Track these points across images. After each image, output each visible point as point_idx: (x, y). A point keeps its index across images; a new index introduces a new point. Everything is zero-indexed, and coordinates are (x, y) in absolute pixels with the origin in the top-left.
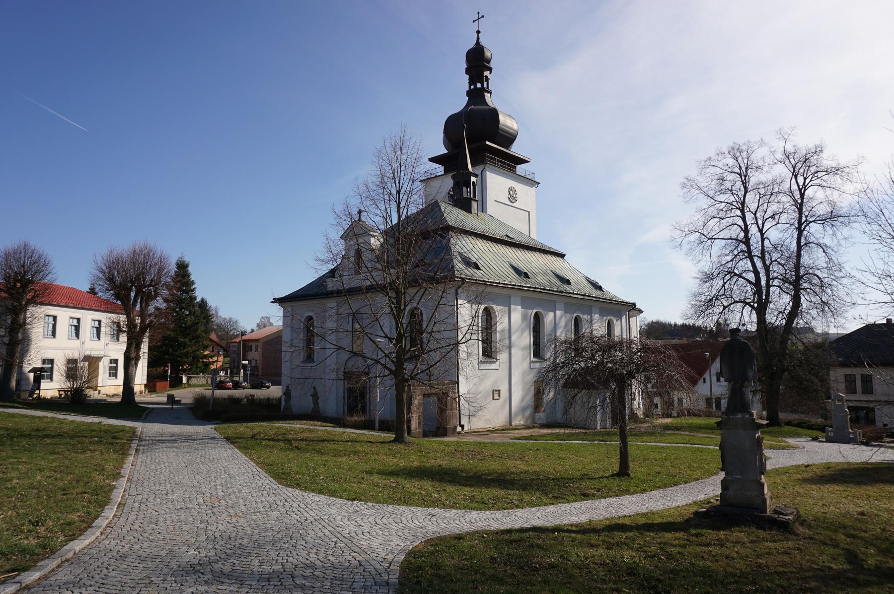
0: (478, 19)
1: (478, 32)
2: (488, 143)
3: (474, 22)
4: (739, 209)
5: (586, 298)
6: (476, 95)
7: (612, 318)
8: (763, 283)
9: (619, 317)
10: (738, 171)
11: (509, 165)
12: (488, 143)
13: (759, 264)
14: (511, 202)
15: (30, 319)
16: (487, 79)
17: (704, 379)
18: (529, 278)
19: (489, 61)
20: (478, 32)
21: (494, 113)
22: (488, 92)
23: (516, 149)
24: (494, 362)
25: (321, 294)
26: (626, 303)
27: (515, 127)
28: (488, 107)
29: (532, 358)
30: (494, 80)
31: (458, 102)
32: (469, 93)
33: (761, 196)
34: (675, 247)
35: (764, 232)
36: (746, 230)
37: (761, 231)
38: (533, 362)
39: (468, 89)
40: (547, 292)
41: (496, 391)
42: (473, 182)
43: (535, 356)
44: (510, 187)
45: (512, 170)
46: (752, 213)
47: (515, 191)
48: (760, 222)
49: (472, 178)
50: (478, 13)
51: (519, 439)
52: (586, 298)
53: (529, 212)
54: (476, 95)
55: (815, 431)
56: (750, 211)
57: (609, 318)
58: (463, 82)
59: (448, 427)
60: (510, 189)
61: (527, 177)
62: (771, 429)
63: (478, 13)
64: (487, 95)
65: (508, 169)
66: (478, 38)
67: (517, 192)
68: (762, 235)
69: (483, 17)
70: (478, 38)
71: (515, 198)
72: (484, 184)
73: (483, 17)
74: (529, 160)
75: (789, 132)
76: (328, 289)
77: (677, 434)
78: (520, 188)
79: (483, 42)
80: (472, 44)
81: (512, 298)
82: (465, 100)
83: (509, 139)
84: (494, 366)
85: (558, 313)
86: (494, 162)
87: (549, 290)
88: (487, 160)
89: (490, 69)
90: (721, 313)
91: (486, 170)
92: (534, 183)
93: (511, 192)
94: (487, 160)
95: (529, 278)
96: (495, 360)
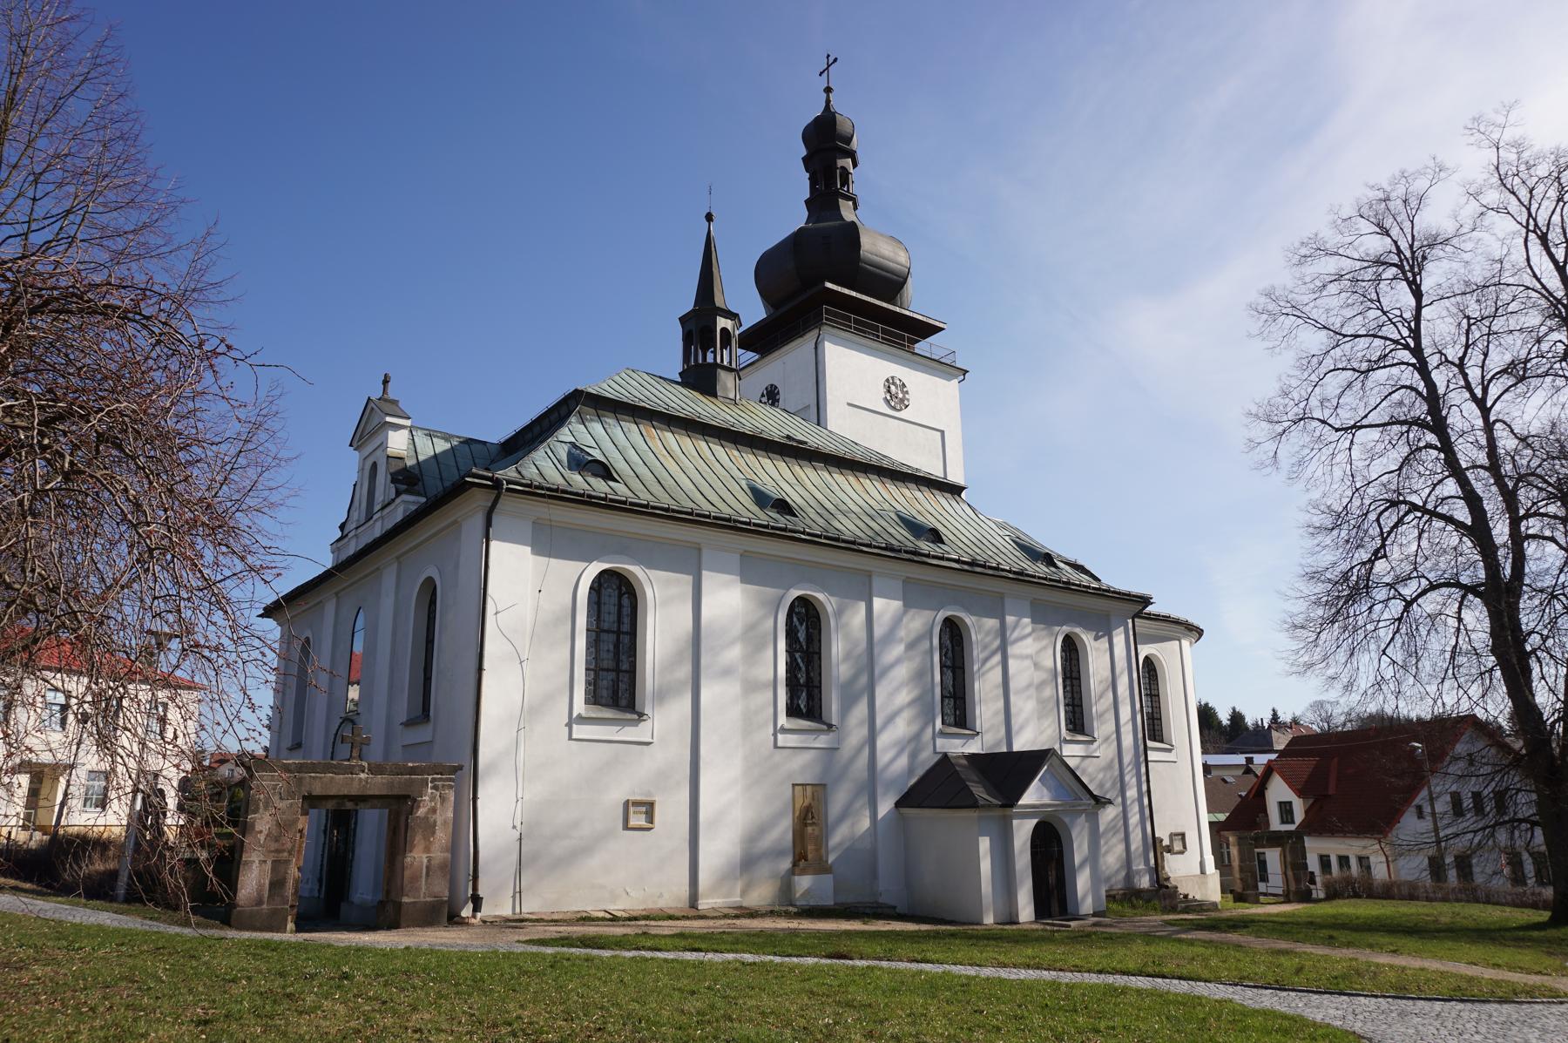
0: (827, 68)
1: (828, 90)
2: (829, 285)
4: (1406, 347)
5: (979, 569)
7: (1078, 630)
8: (1501, 531)
9: (1104, 629)
10: (1396, 260)
11: (856, 322)
12: (829, 285)
13: (1482, 483)
14: (894, 408)
17: (1419, 809)
18: (795, 516)
19: (849, 140)
20: (828, 90)
21: (852, 232)
22: (848, 198)
24: (635, 723)
26: (1119, 593)
27: (902, 258)
29: (783, 720)
30: (862, 179)
33: (1472, 321)
34: (1262, 465)
35: (1489, 404)
36: (1433, 398)
37: (1481, 403)
38: (784, 730)
41: (637, 804)
42: (724, 330)
43: (792, 711)
44: (888, 376)
46: (1452, 363)
47: (904, 385)
48: (1478, 392)
50: (828, 56)
51: (542, 942)
52: (979, 569)
53: (942, 432)
55: (1526, 911)
56: (1447, 360)
57: (1066, 629)
59: (405, 900)
60: (889, 382)
61: (942, 360)
62: (1552, 933)
63: (828, 56)
65: (855, 329)
66: (828, 102)
67: (909, 387)
68: (1485, 411)
69: (835, 60)
70: (828, 102)
71: (902, 401)
72: (820, 369)
74: (941, 325)
75: (1501, 120)
77: (1228, 944)
78: (916, 381)
79: (836, 106)
81: (706, 555)
82: (804, 214)
83: (891, 284)
84: (630, 733)
85: (878, 603)
86: (843, 324)
88: (827, 319)
89: (852, 155)
90: (1400, 619)
91: (823, 340)
92: (956, 372)
93: (893, 388)
94: (827, 319)
95: (795, 516)
96: (636, 717)
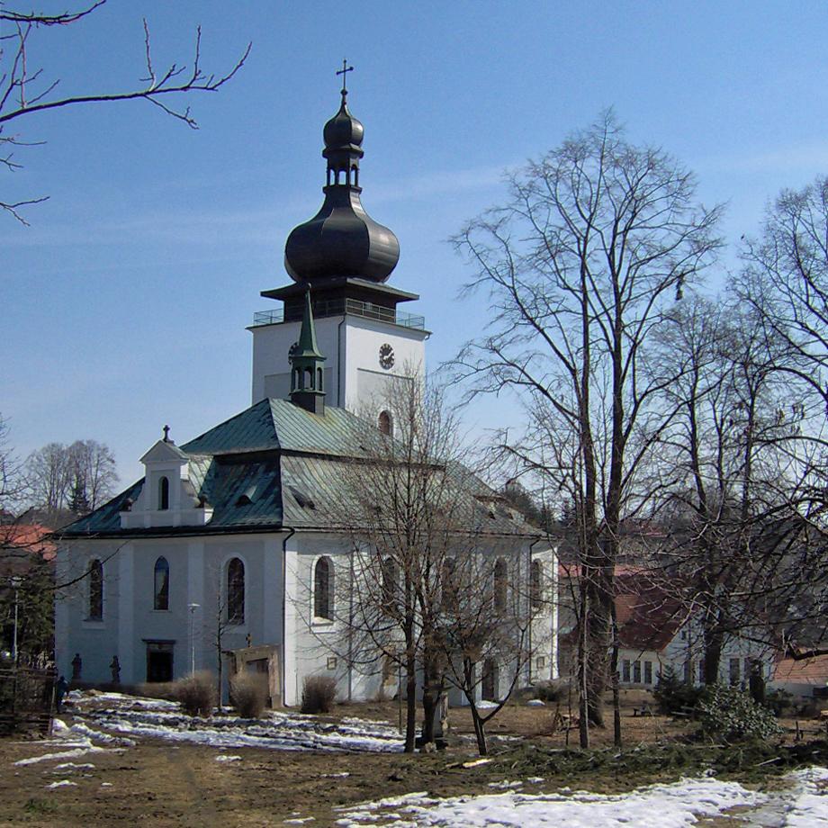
1: (344, 93)
2: (349, 280)
3: (338, 73)
6: (338, 197)
14: (384, 367)
15: (642, 494)
16: (355, 168)
20: (344, 93)
23: (394, 283)
25: (114, 533)
28: (353, 219)
30: (369, 170)
31: (308, 206)
32: (327, 190)
39: (325, 185)
40: (305, 530)
45: (387, 319)
49: (317, 362)
50: (345, 62)
54: (338, 197)
58: (317, 173)
63: (345, 62)
64: (353, 197)
66: (344, 103)
69: (351, 69)
73: (351, 69)
76: (122, 526)
80: (332, 113)
87: (309, 528)
92: (422, 334)
